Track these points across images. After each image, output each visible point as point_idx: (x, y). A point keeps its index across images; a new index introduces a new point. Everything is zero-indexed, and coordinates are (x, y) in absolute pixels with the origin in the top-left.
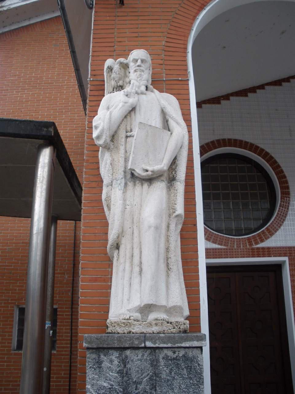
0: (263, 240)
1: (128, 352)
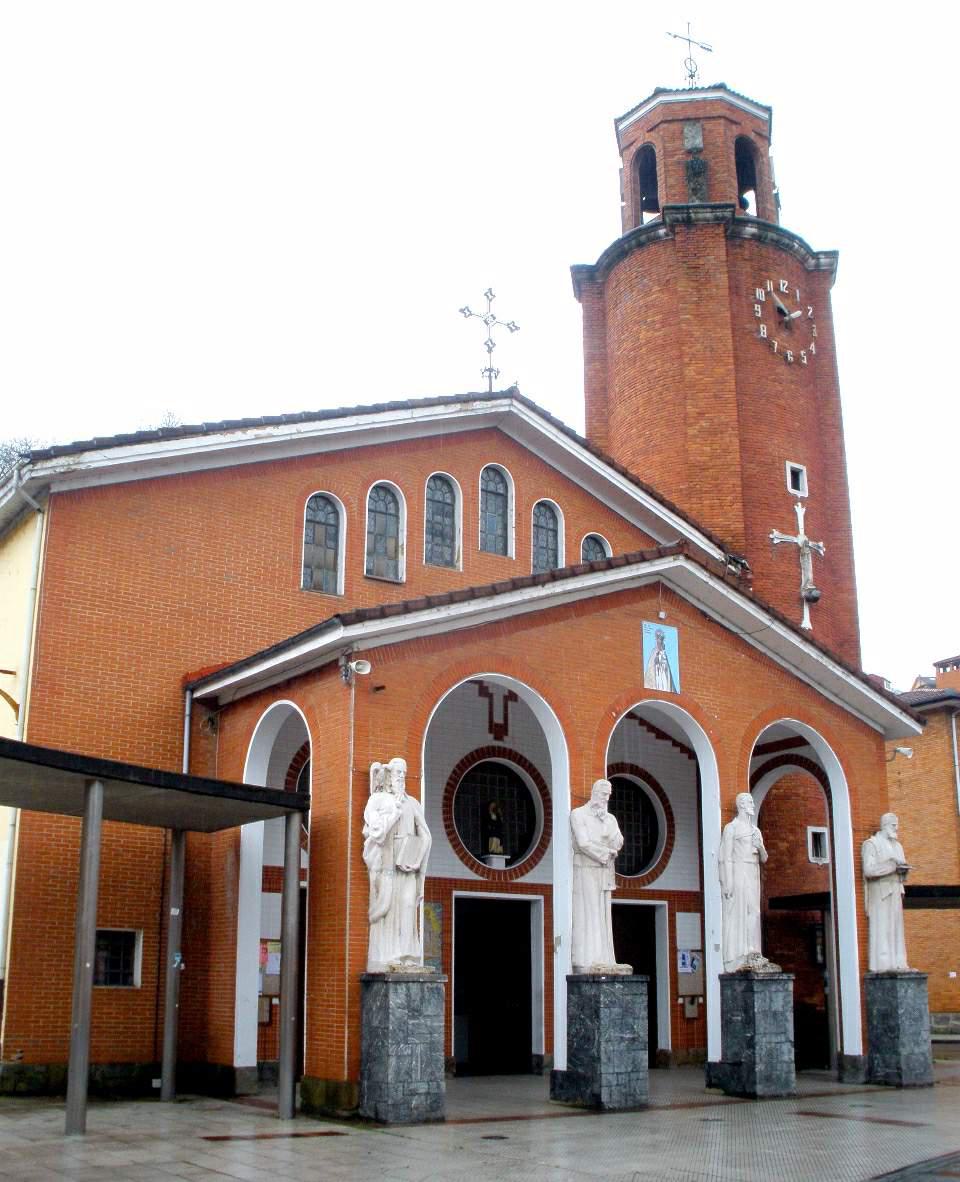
1: (411, 984)
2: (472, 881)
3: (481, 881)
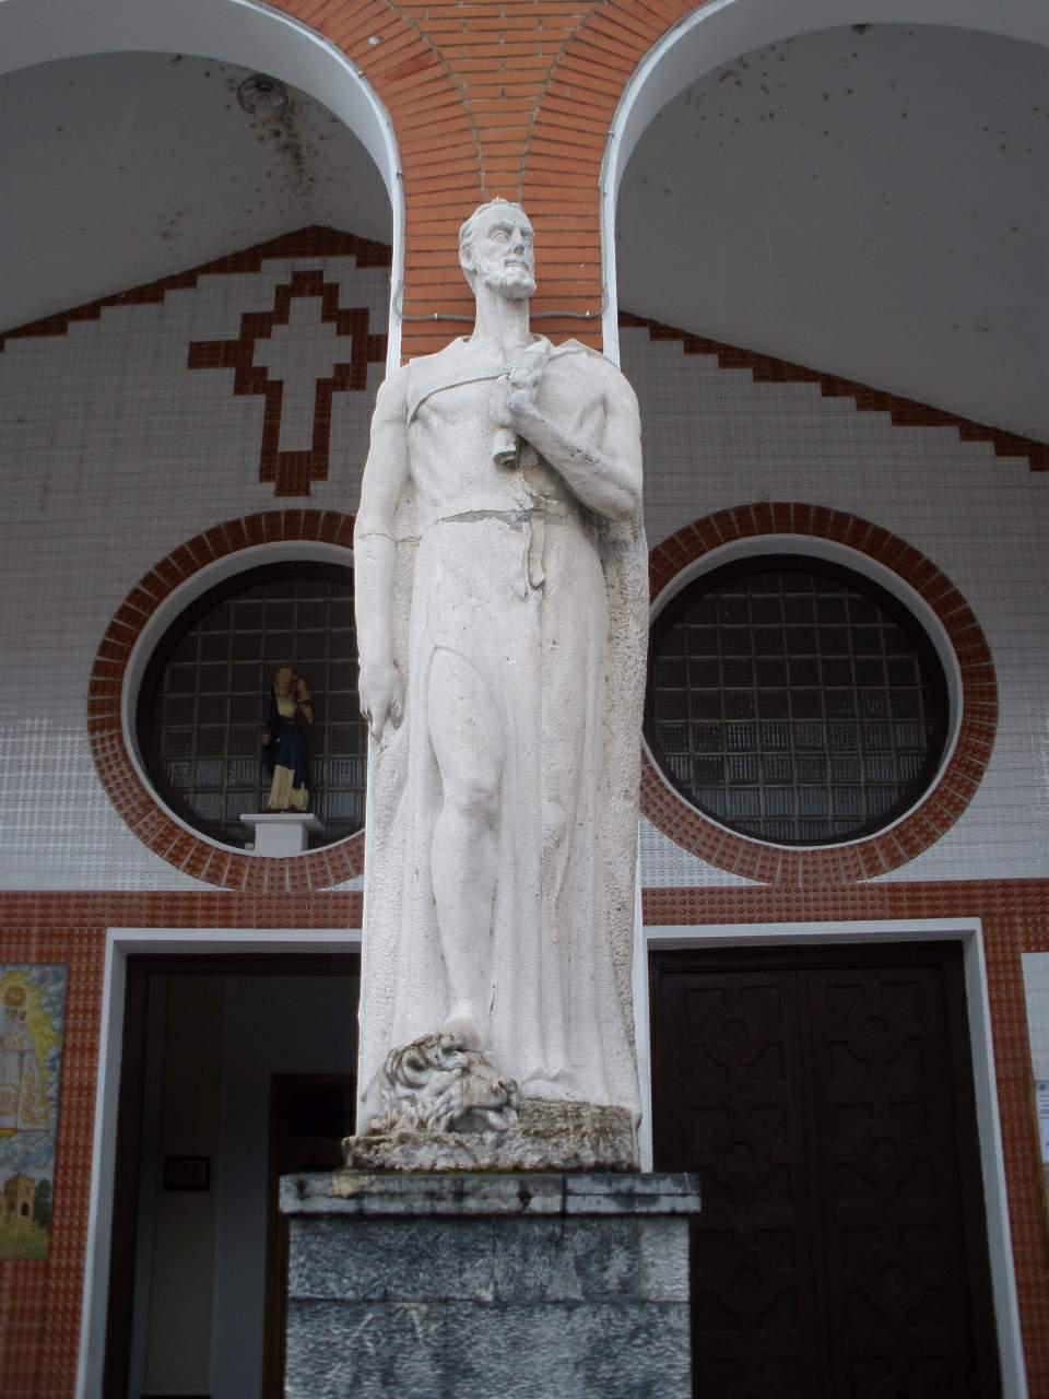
2: (173, 897)
3: (209, 897)
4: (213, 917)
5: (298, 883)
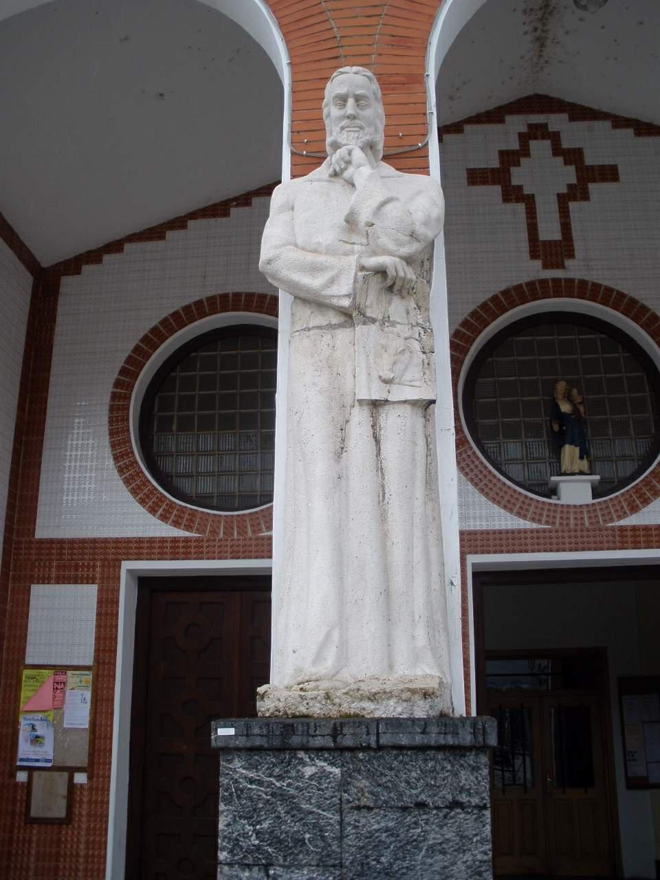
0: (168, 518)
2: (163, 540)
3: (187, 540)
4: (154, 554)
5: (594, 521)
